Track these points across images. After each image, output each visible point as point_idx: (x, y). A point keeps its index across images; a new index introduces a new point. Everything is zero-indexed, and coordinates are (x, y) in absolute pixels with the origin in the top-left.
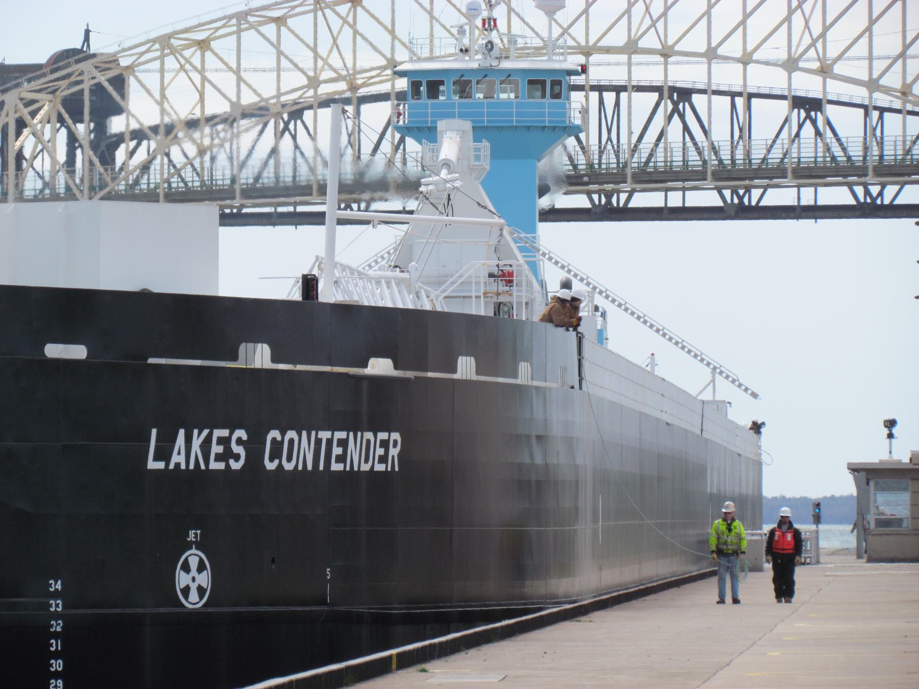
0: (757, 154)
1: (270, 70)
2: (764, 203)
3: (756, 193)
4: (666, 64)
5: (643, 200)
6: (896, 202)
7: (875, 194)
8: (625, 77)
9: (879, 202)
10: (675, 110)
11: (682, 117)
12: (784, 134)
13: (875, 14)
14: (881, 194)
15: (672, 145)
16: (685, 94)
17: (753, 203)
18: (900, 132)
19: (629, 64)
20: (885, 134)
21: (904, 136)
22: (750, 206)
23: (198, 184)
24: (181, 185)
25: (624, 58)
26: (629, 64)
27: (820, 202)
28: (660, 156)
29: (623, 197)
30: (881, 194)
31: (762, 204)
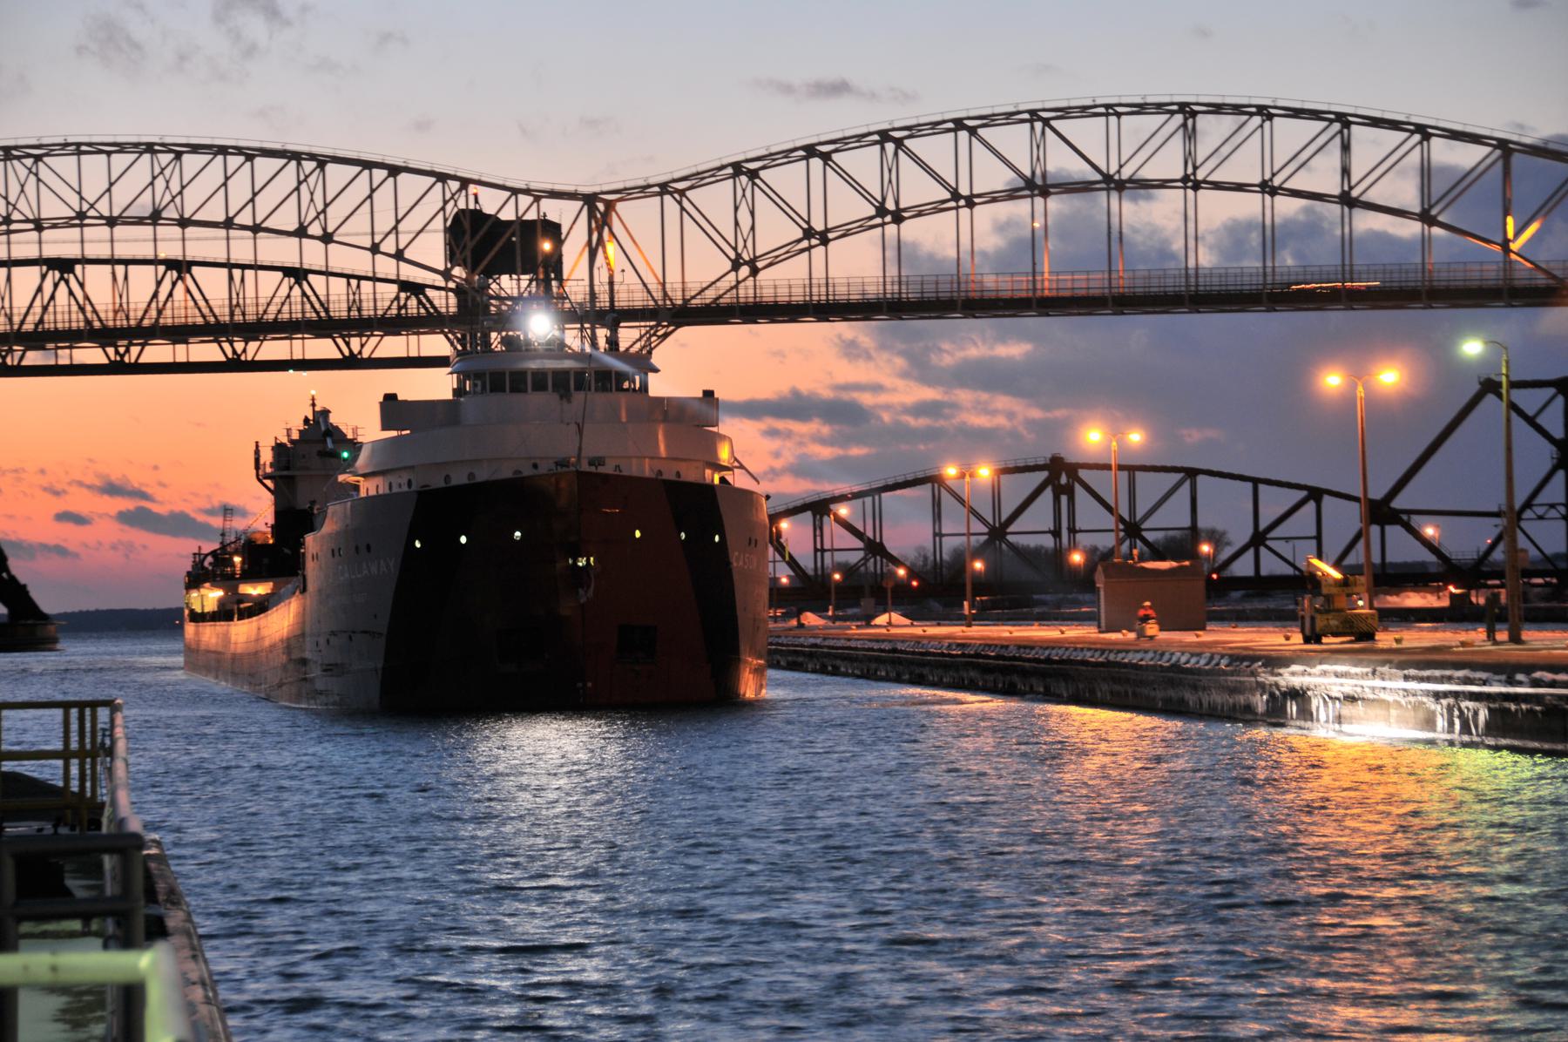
0: (135, 315)
1: (366, 234)
2: (143, 360)
3: (135, 350)
4: (255, 238)
5: (33, 358)
6: (373, 356)
7: (239, 352)
8: (109, 253)
9: (243, 358)
10: (62, 278)
11: (67, 282)
12: (38, 303)
13: (368, 201)
14: (244, 351)
15: (836, 281)
16: (64, 266)
17: (133, 361)
18: (896, 274)
19: (9, 243)
20: (14, 305)
21: (900, 276)
22: (13, 366)
23: (82, 324)
24: (314, 315)
25: (222, 232)
26: (9, 243)
27: (192, 359)
28: (49, 317)
29: (17, 355)
30: (244, 351)
31: (141, 361)
